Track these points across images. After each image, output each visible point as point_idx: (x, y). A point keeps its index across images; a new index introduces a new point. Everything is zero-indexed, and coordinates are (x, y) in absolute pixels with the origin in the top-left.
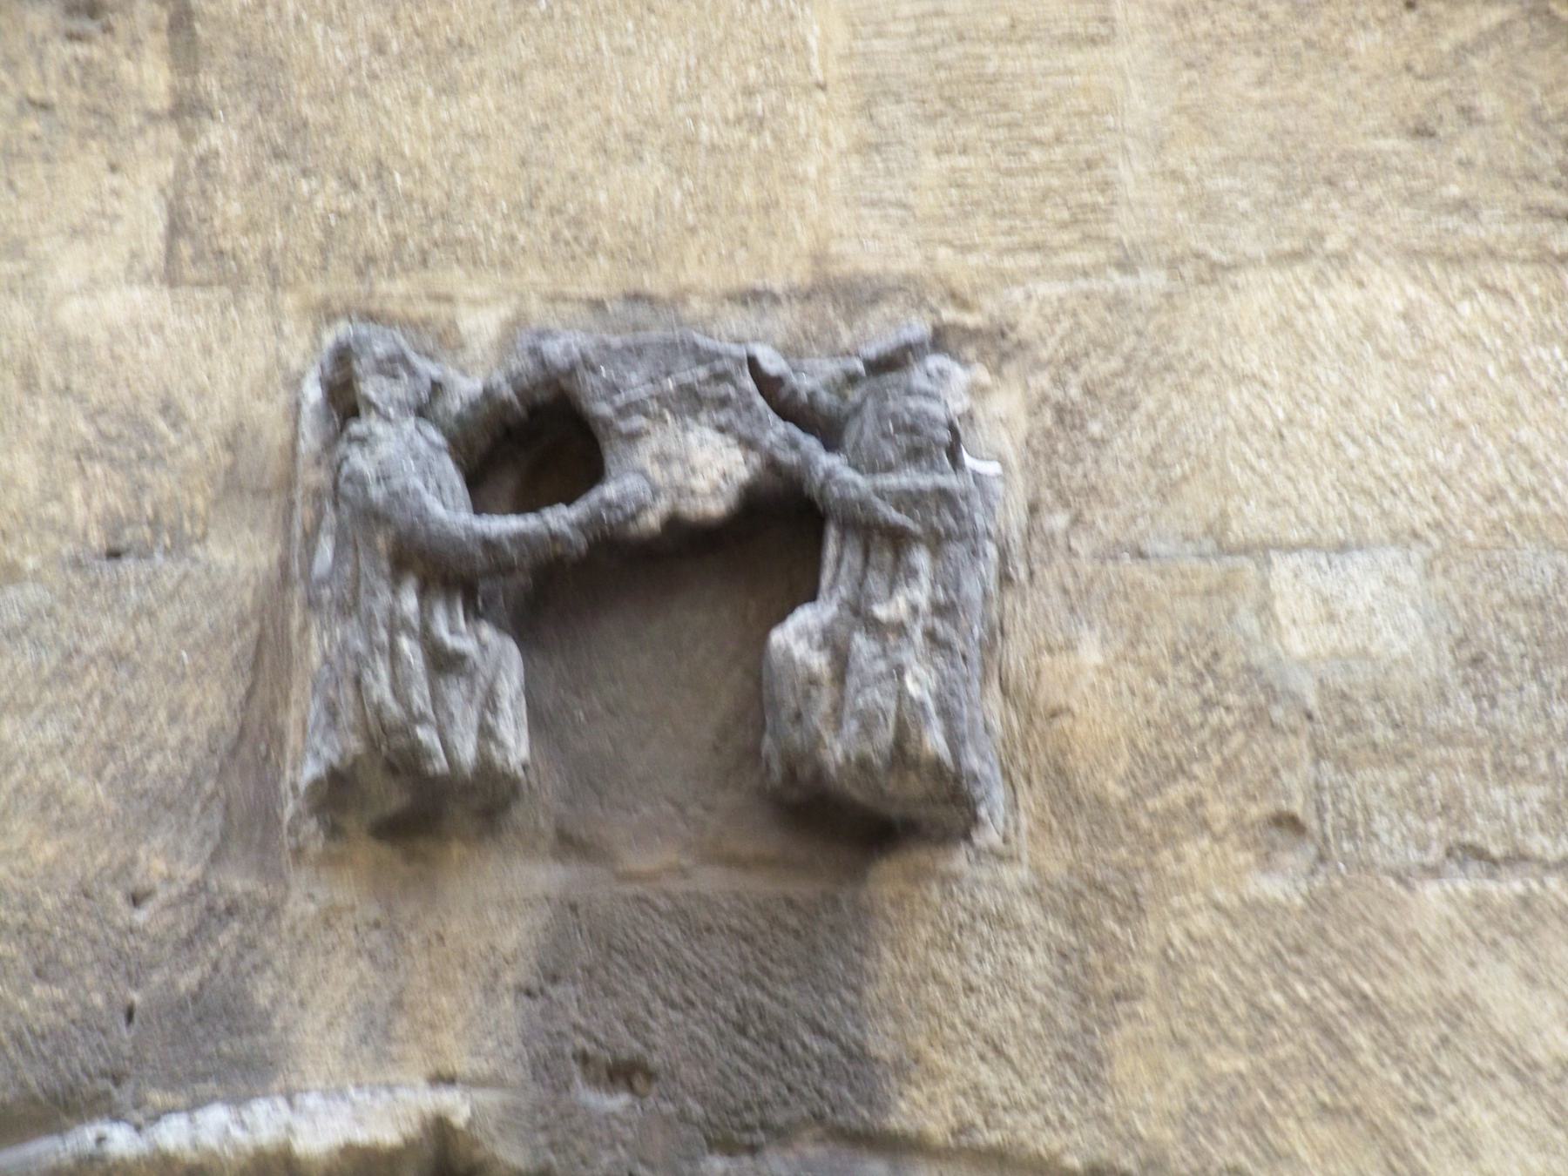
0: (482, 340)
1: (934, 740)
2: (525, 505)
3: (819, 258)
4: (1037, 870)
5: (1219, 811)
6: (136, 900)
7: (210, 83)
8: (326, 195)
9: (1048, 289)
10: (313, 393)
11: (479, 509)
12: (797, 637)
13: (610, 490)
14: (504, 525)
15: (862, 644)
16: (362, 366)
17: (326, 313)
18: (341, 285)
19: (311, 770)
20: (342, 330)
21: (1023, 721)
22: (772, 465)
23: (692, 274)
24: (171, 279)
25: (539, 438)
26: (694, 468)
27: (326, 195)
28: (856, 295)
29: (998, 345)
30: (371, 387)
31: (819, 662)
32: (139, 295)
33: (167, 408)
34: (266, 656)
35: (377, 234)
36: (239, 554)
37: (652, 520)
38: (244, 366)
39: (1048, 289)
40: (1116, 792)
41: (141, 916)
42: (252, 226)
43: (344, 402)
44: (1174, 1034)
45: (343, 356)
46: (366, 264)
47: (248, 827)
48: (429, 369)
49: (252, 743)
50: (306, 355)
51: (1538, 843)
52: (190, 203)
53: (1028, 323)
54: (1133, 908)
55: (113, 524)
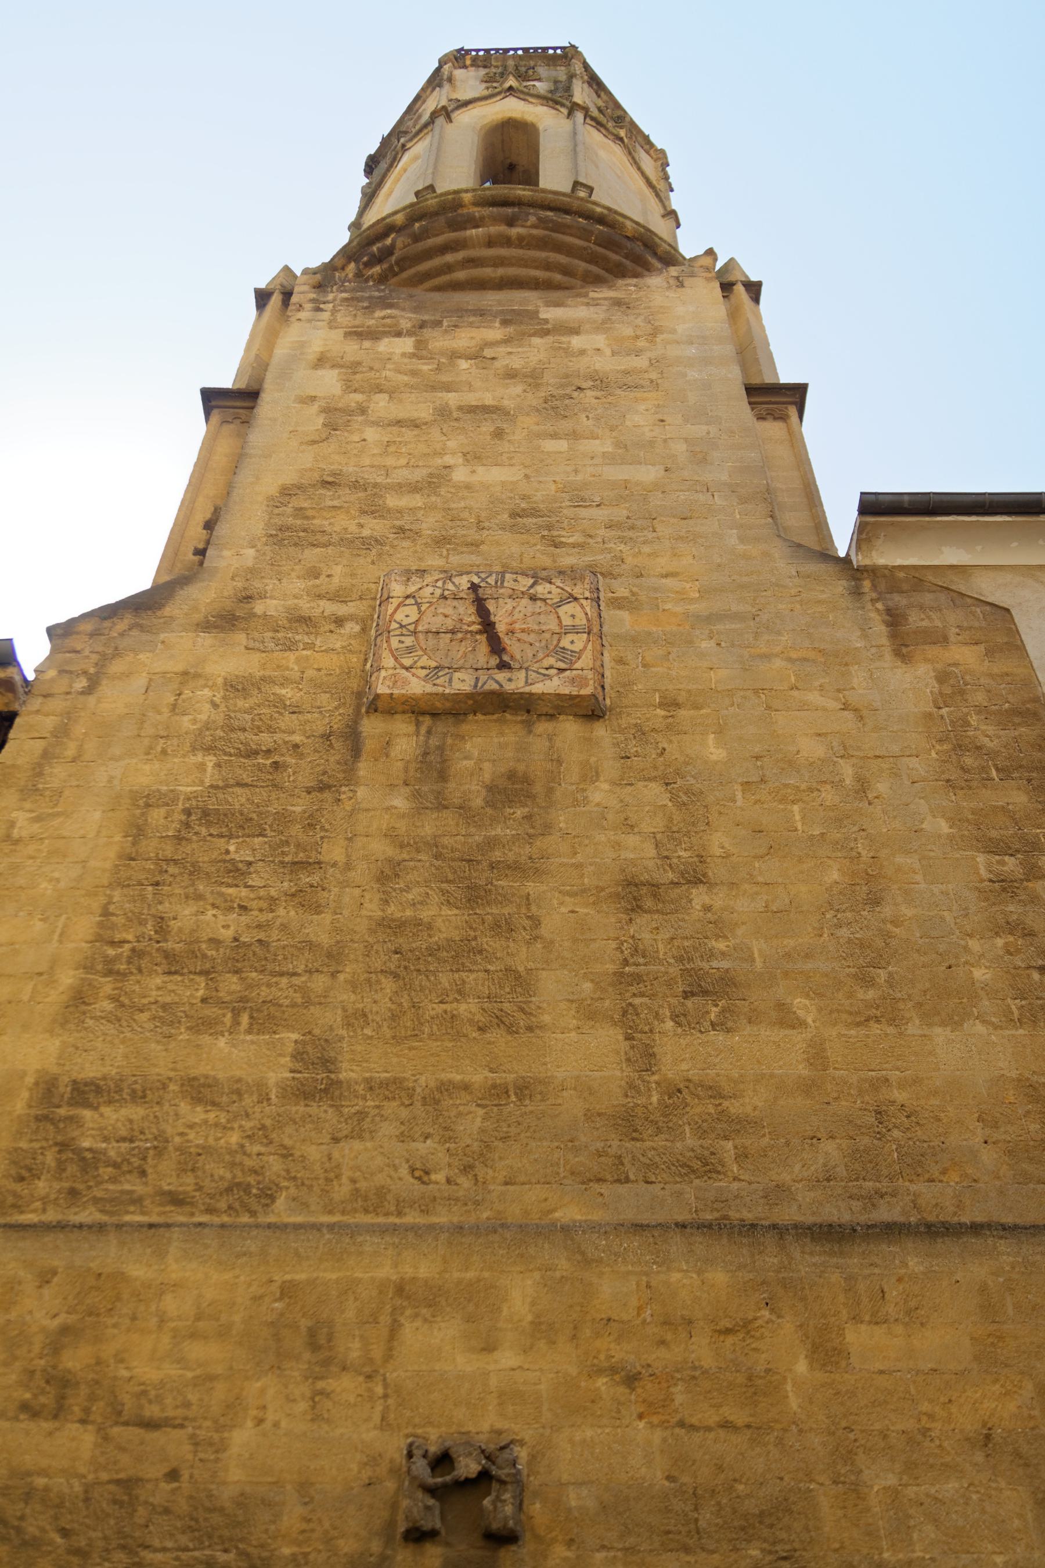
0: (434, 1441)
1: (511, 1523)
2: (442, 1476)
3: (492, 1426)
4: (817, 1055)
5: (560, 1538)
6: (371, 1556)
7: (389, 1391)
8: (408, 1413)
9: (531, 1432)
10: (405, 1452)
11: (433, 1477)
12: (487, 1502)
13: (455, 1473)
14: (439, 1480)
15: (499, 1504)
16: (413, 1447)
17: (407, 1436)
18: (410, 1430)
19: (403, 1529)
20: (410, 1440)
21: (132, 1208)
22: (483, 1467)
23: (470, 1429)
24: (381, 1428)
25: (443, 1460)
26: (468, 1467)
27: (408, 1413)
28: (499, 1432)
29: (521, 1443)
30: (415, 1452)
31: (491, 1508)
32: (376, 1432)
33: (380, 1455)
34: (394, 1506)
35: (417, 1420)
36: (390, 1485)
37: (462, 1478)
38: (394, 1447)
39: (531, 1432)
40: (542, 1534)
41: (372, 1559)
42: (396, 1419)
43: (410, 1455)
44: (314, 442)
45: (411, 1445)
46: (415, 1426)
47: (389, 1541)
48: (425, 1447)
49: (391, 1524)
50: (403, 1444)
51: (615, 1545)
52: (124, 1229)
53: (527, 1439)
54: (545, 1557)
55: (370, 1478)
